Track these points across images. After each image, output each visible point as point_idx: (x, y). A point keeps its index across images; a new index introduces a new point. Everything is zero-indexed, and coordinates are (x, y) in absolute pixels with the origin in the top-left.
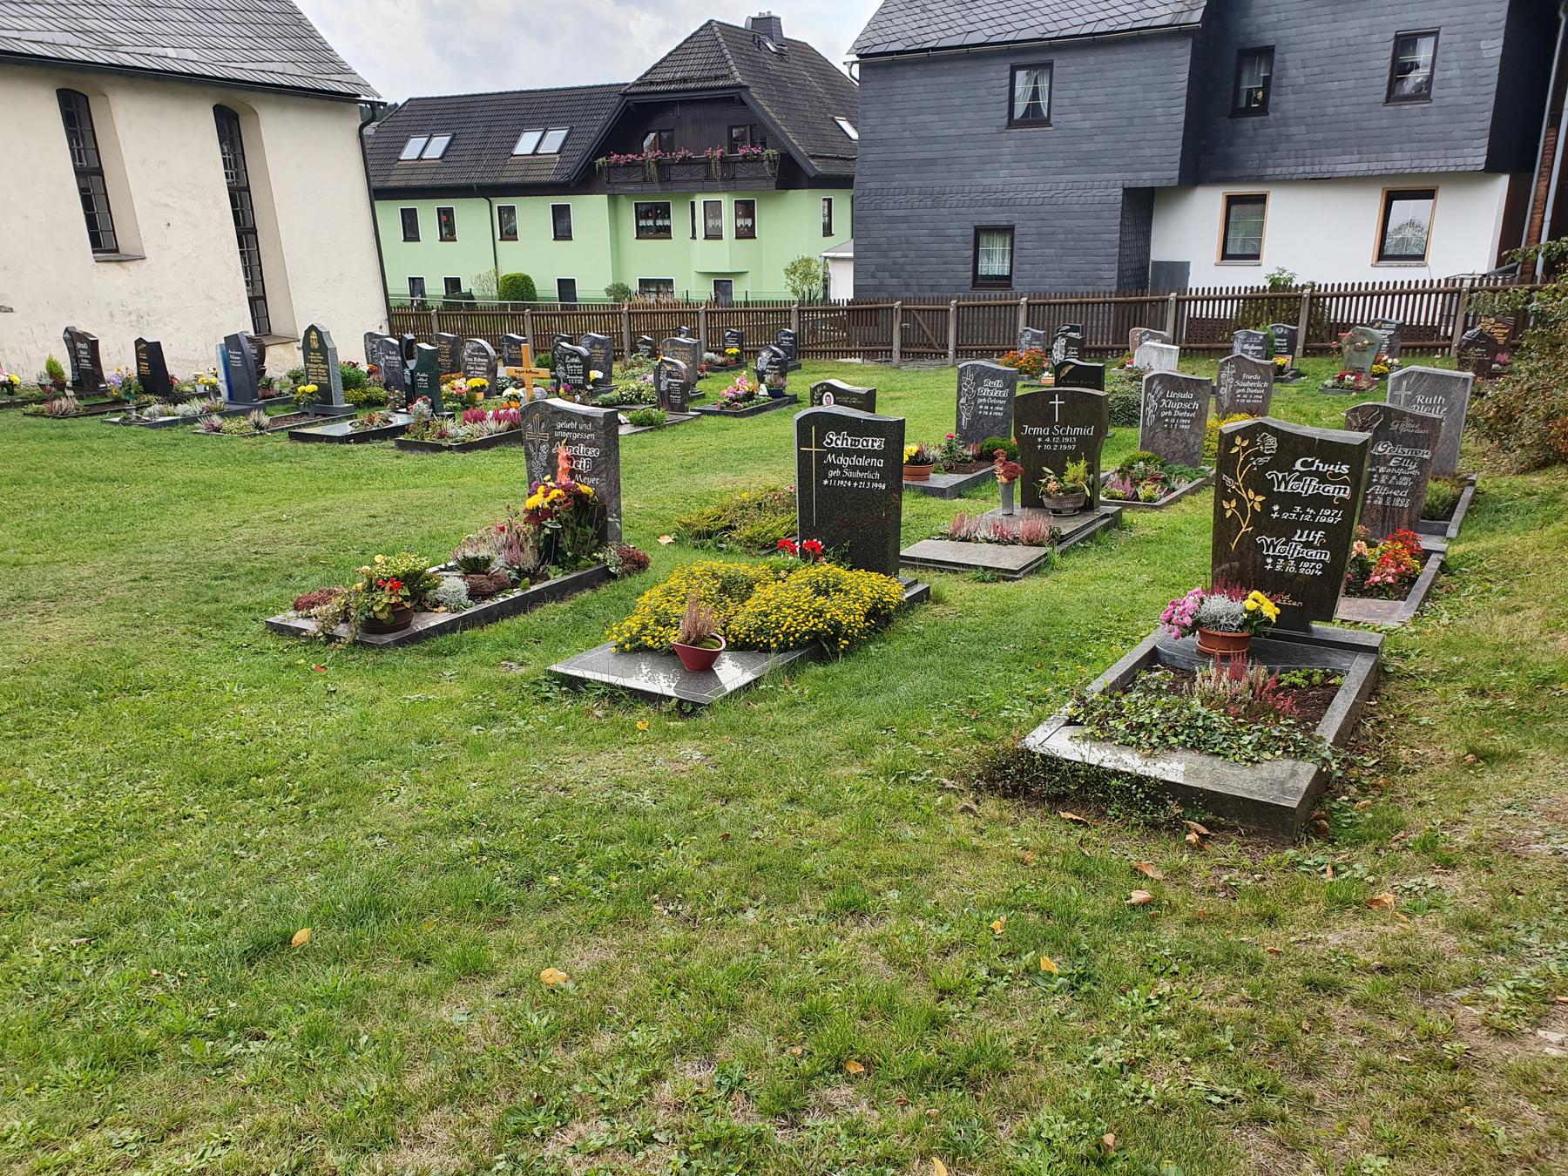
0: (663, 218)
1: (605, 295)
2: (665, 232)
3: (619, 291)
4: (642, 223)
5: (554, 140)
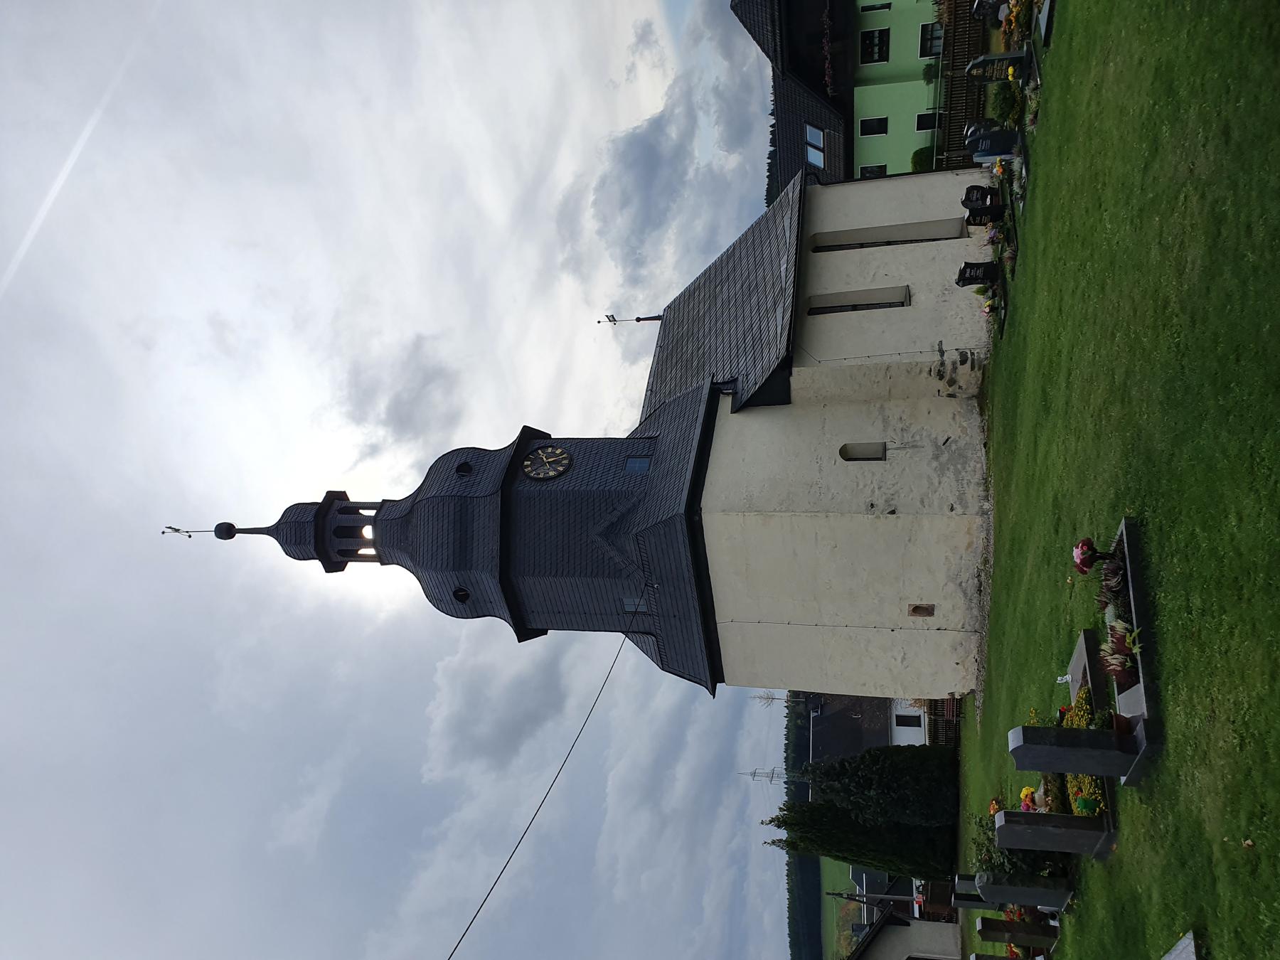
0: (873, 37)
1: (932, 86)
2: (885, 34)
3: (929, 74)
4: (876, 56)
5: (814, 135)
